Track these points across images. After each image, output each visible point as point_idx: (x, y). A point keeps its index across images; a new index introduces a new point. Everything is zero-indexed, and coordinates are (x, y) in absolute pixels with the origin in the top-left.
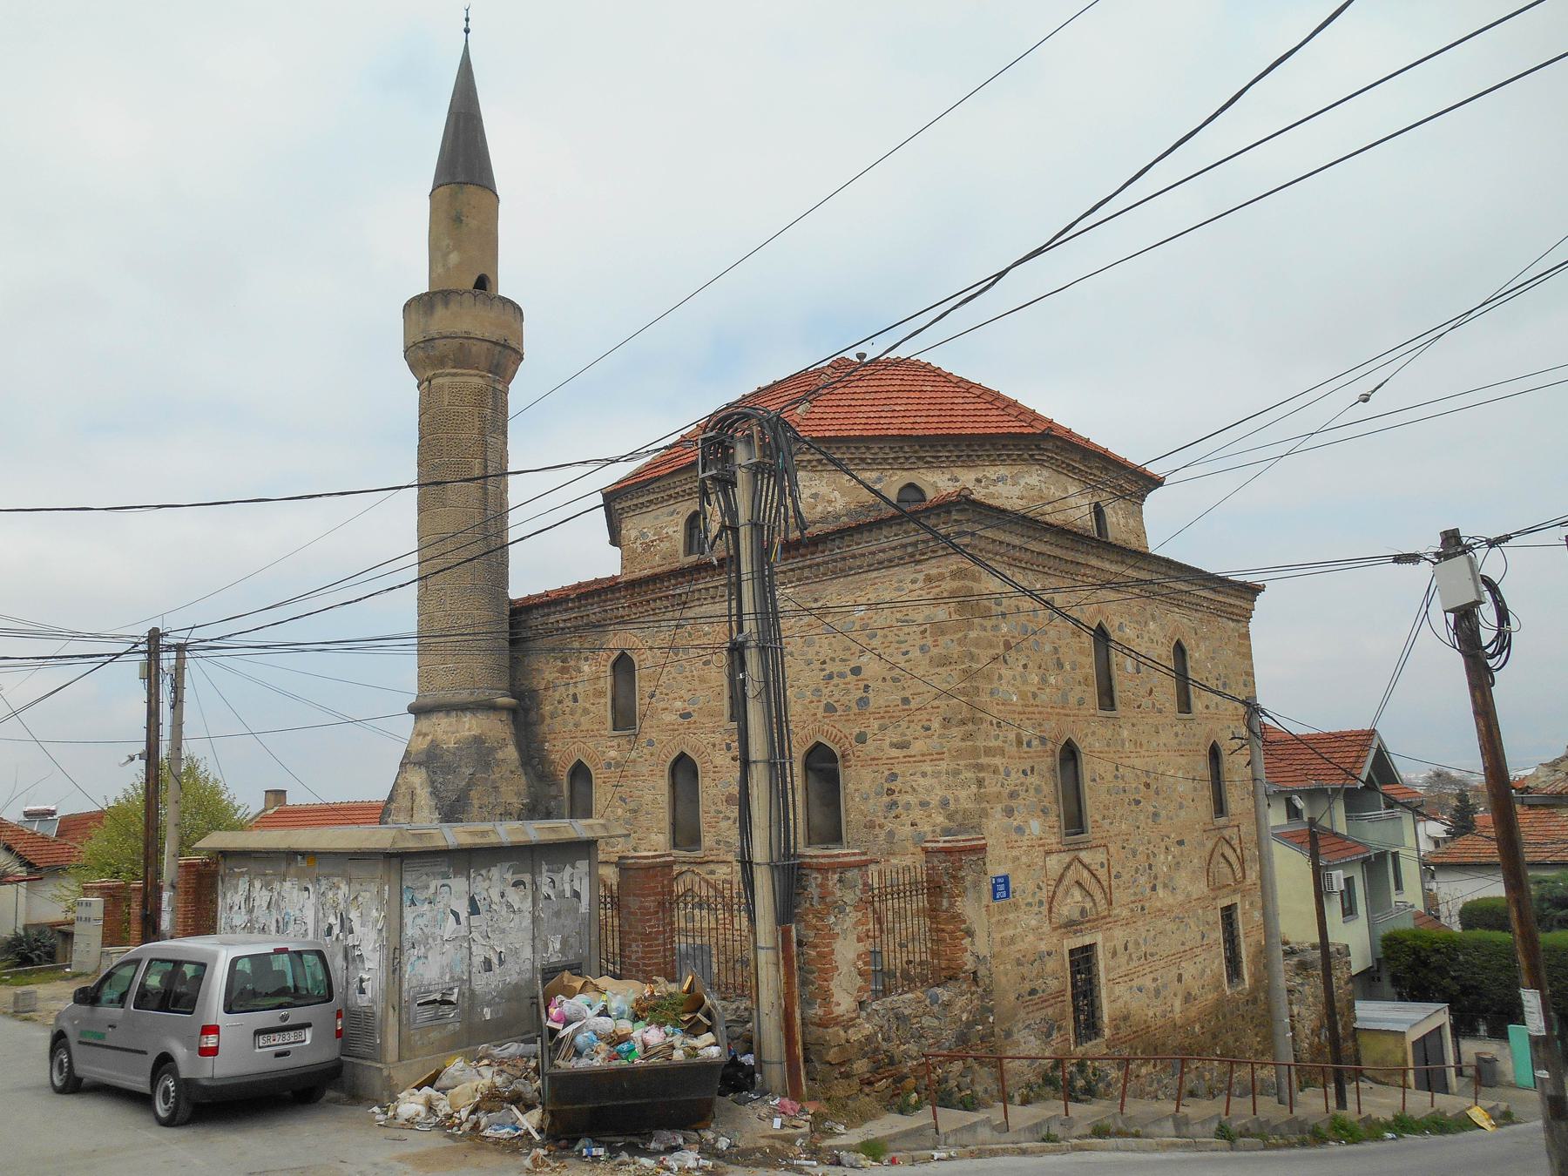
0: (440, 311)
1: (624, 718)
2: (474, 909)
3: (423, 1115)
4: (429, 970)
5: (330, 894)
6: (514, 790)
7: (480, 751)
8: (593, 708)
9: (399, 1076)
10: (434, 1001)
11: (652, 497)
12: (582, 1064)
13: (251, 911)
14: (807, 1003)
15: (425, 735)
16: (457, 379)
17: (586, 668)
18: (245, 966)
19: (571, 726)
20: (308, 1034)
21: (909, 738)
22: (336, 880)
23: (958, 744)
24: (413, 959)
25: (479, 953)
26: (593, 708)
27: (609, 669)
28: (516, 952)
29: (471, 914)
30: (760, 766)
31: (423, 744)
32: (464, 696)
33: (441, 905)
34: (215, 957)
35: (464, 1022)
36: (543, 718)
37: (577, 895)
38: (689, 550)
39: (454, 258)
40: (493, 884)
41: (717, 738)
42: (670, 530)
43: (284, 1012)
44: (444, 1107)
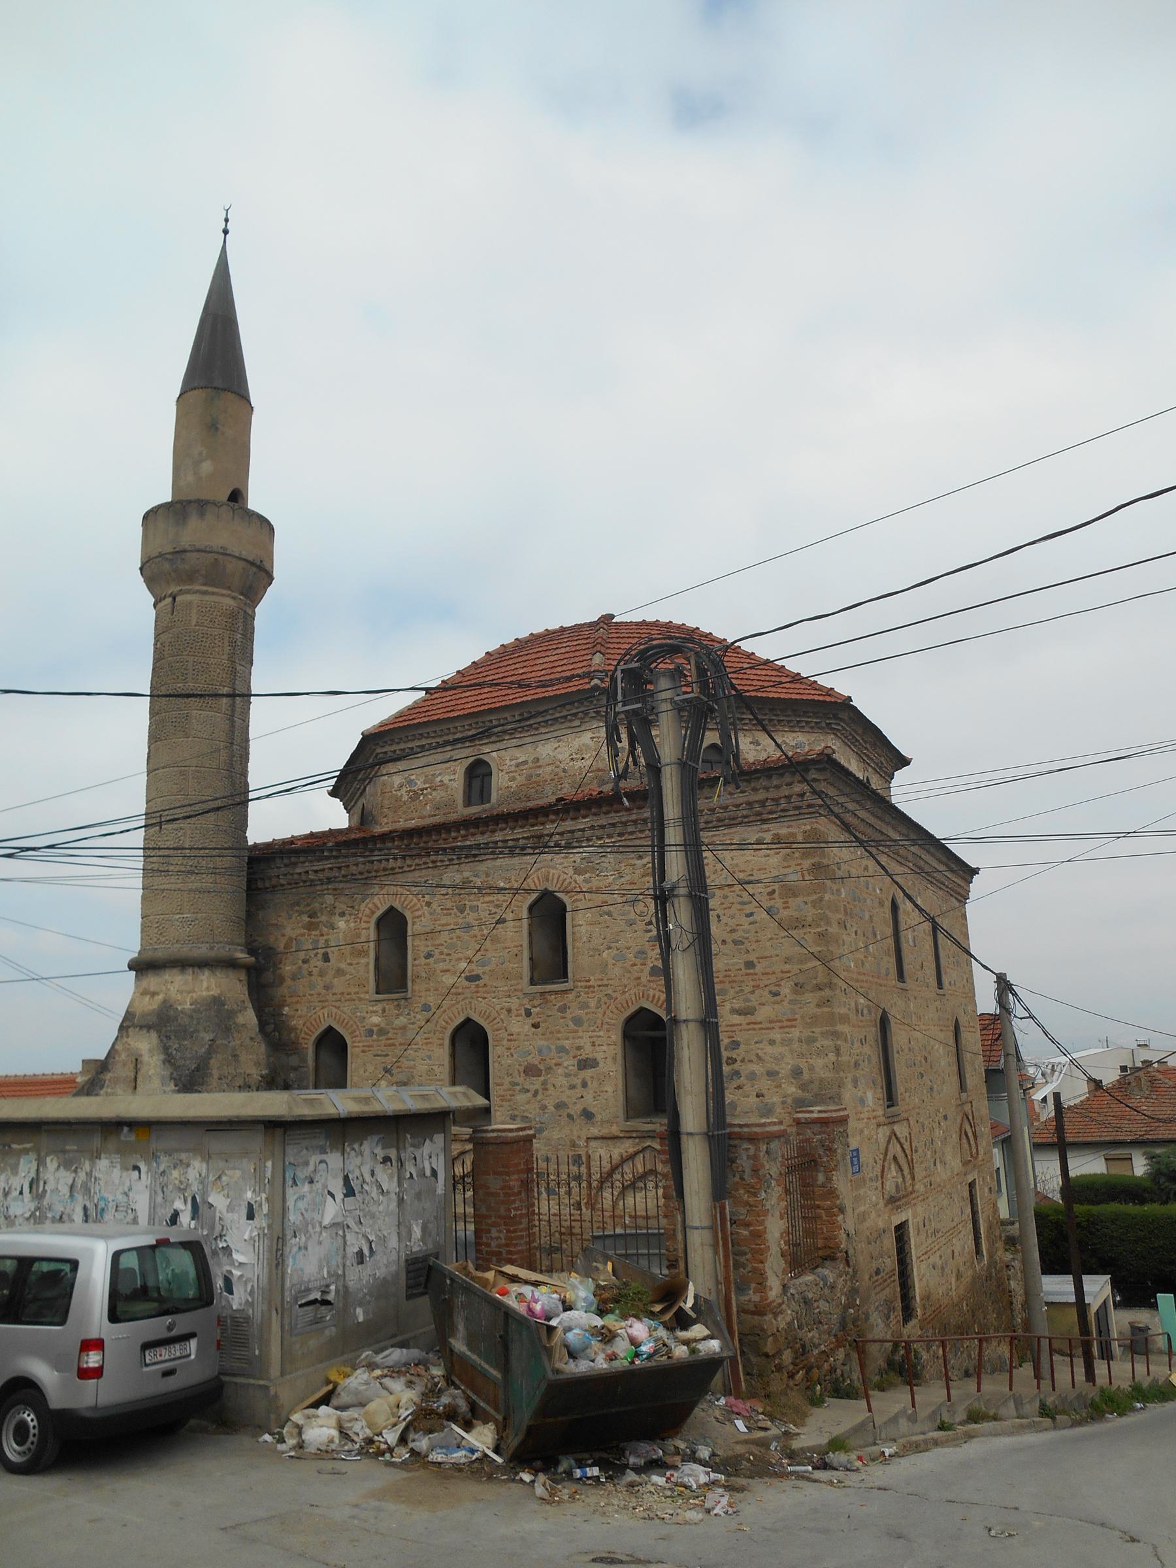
0: (194, 522)
1: (393, 978)
2: (350, 1192)
3: (337, 1441)
4: (309, 1265)
5: (175, 1174)
6: (253, 1058)
7: (218, 1013)
8: (350, 969)
9: (285, 1395)
10: (315, 1302)
11: (424, 742)
12: (581, 1367)
13: (40, 1197)
14: (741, 1289)
15: (154, 994)
16: (207, 598)
17: (342, 924)
18: (130, 1262)
19: (319, 989)
20: (193, 1343)
21: (755, 1004)
22: (183, 1156)
23: (812, 1009)
24: (295, 1249)
25: (355, 1243)
26: (350, 969)
27: (372, 926)
28: (383, 1240)
29: (346, 1196)
30: (692, 1026)
31: (150, 1005)
32: (202, 951)
33: (319, 1186)
34: (91, 1253)
35: (343, 1329)
36: (282, 980)
37: (434, 1173)
38: (468, 802)
39: (207, 467)
40: (364, 1159)
41: (514, 1003)
42: (446, 779)
43: (168, 1319)
44: (360, 1430)
